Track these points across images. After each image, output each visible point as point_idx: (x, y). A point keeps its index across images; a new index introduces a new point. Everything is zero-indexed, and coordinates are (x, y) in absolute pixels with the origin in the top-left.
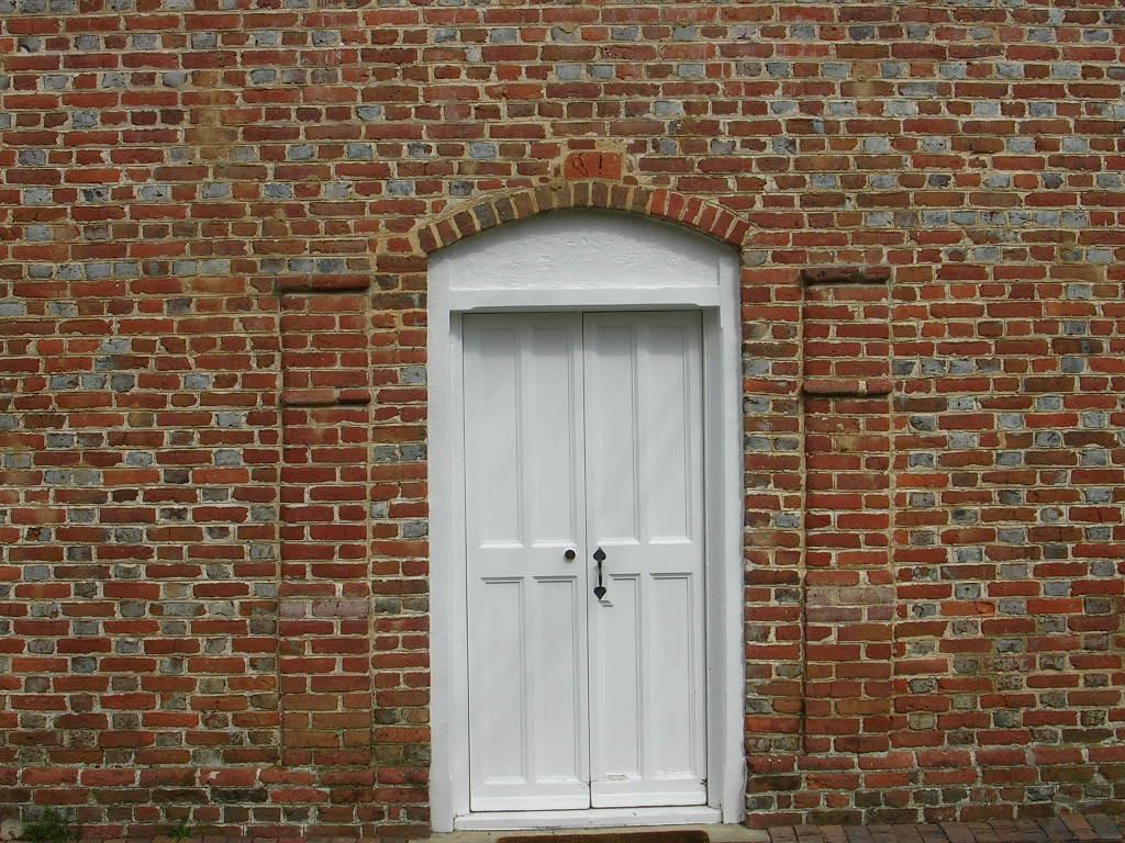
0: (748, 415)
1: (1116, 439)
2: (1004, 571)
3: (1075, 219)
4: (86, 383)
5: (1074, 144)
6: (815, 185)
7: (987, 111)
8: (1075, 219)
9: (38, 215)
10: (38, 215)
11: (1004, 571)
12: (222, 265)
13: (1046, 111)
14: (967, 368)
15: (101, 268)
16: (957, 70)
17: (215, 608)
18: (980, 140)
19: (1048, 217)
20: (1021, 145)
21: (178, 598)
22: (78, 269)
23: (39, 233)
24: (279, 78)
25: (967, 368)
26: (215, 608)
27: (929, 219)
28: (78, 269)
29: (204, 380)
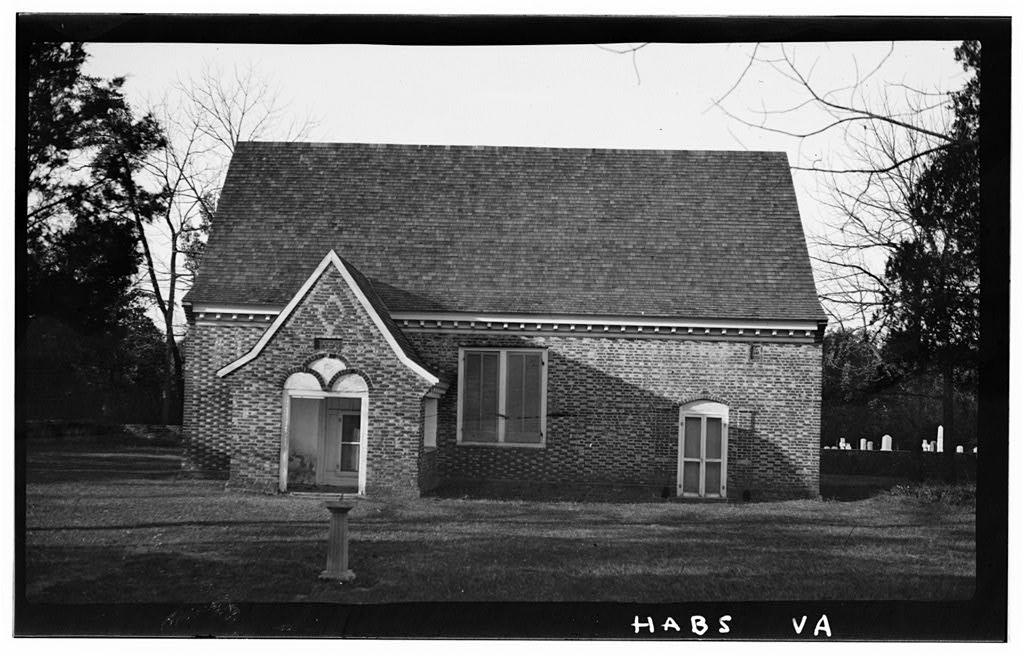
0: (681, 408)
1: (67, 90)
2: (769, 459)
3: (783, 403)
4: (626, 423)
5: (784, 391)
6: (742, 397)
7: (769, 386)
8: (783, 403)
9: (608, 390)
10: (608, 390)
11: (769, 459)
12: (647, 406)
13: (778, 385)
14: (764, 427)
15: (629, 405)
16: (764, 379)
17: (644, 459)
18: (768, 390)
19: (778, 403)
20: (774, 391)
21: (638, 458)
22: (624, 405)
23: (619, 399)
24: (658, 377)
25: (764, 427)
26: (644, 459)
27: (760, 402)
28: (624, 405)
29: (644, 423)
